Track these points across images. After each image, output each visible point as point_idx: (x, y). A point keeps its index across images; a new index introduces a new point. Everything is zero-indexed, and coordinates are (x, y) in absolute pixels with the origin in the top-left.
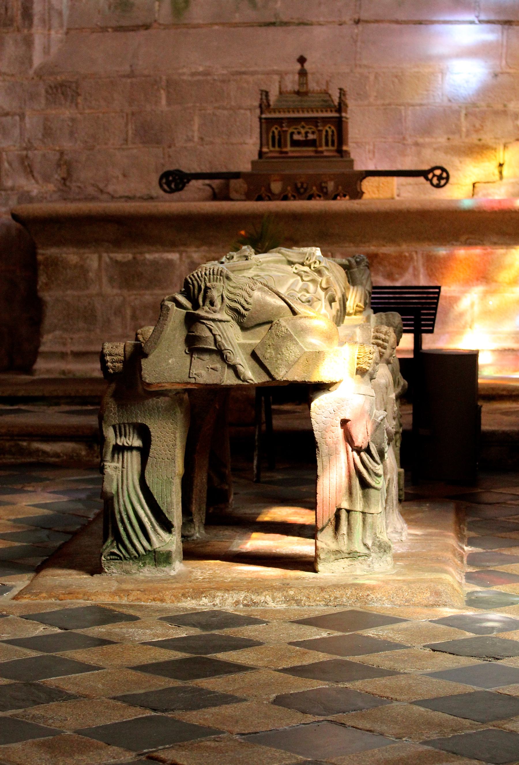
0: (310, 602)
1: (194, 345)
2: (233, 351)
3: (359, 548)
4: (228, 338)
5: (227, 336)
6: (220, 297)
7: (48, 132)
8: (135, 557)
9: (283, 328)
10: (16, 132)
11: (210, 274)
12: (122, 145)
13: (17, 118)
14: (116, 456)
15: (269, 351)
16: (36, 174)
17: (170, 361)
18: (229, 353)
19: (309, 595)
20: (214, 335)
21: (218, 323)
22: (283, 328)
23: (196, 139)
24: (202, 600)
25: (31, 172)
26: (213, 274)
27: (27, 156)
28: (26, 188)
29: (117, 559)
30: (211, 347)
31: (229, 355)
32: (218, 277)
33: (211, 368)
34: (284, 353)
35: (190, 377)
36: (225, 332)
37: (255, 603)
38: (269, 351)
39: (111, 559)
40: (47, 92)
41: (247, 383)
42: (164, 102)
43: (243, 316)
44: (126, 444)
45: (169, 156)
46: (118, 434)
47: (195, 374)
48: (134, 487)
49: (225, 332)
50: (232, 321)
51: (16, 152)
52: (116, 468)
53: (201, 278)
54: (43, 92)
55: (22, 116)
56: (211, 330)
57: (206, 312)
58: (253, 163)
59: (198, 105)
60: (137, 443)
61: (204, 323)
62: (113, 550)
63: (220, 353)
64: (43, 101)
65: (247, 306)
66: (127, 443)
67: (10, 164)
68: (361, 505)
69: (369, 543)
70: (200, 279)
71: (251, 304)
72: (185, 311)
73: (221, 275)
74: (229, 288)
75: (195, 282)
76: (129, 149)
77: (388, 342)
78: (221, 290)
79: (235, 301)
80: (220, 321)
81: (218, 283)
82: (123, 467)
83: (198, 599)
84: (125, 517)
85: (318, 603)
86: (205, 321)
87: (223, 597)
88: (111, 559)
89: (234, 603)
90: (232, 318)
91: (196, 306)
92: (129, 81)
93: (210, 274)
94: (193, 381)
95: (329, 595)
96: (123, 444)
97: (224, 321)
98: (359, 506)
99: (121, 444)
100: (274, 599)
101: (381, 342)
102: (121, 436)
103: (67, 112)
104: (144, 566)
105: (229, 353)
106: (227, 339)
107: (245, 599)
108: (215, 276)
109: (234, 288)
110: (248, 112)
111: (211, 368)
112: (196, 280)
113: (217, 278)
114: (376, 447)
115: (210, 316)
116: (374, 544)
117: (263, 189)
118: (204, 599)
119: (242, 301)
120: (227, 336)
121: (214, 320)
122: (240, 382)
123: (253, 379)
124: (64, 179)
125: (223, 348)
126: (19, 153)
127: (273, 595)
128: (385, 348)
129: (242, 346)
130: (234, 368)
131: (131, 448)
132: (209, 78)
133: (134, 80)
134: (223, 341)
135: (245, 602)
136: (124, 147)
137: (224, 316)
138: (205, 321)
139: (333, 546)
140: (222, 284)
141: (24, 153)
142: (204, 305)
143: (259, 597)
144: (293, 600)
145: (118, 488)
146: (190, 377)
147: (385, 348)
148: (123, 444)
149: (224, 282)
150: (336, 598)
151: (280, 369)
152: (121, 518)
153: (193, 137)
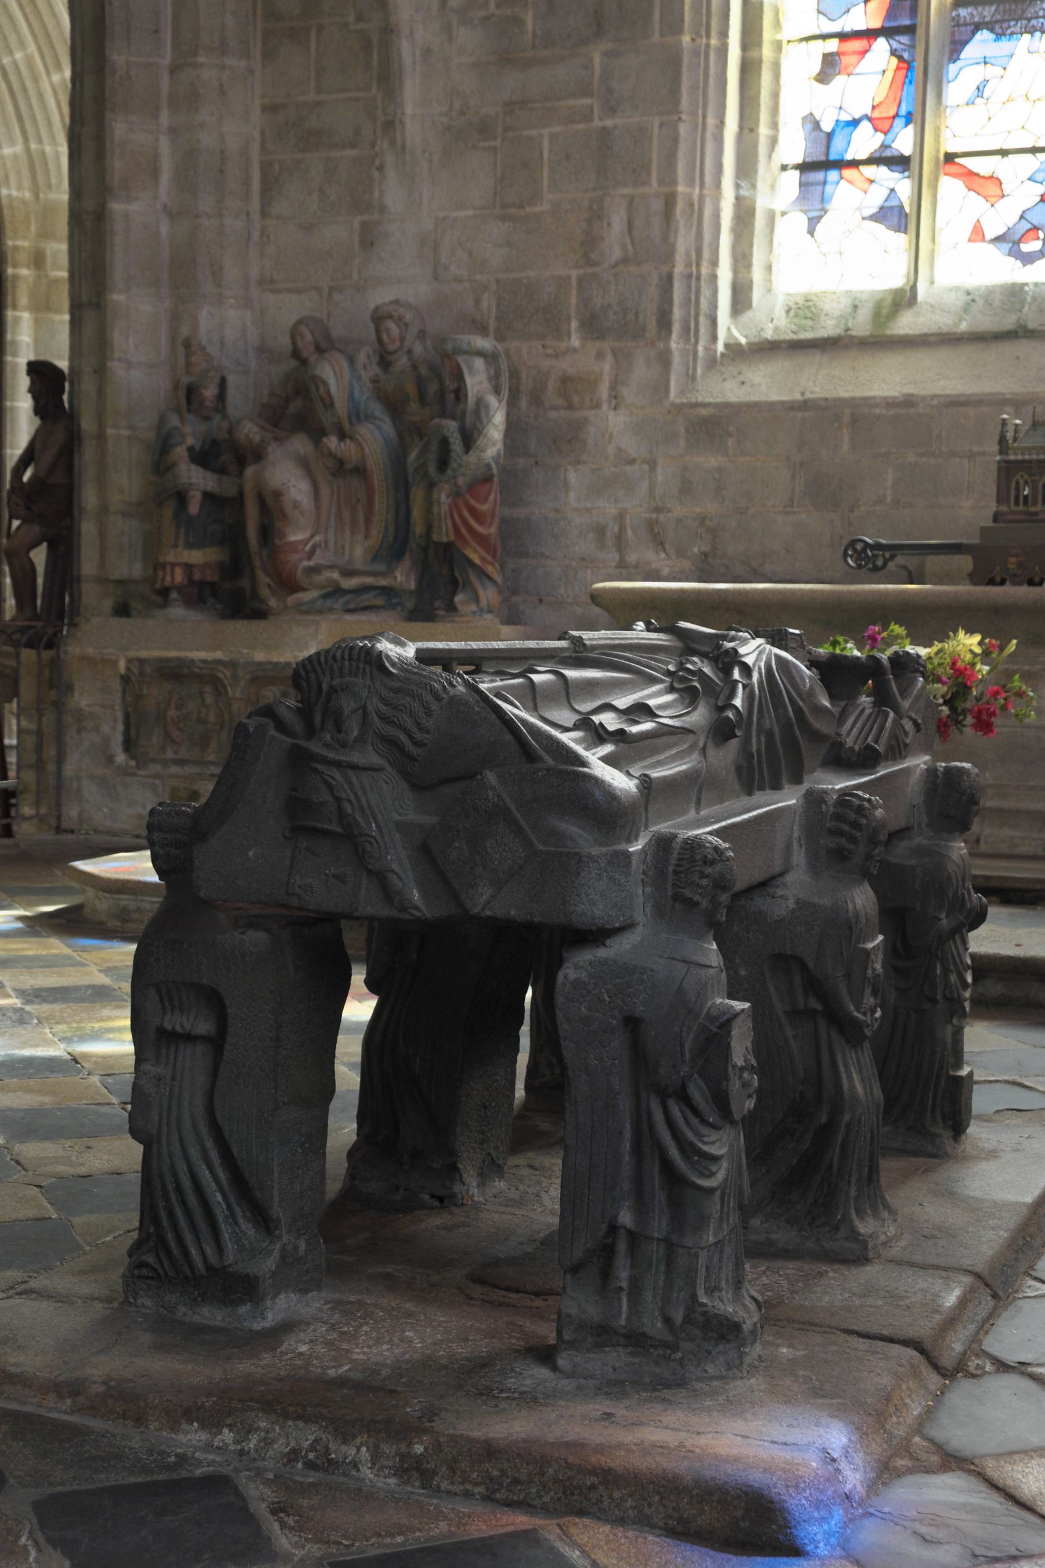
0: (452, 1483)
1: (302, 820)
2: (379, 839)
3: (653, 1326)
4: (370, 808)
5: (368, 803)
6: (361, 711)
7: (686, 489)
8: (186, 1277)
9: (490, 793)
10: (644, 486)
11: (343, 658)
12: (785, 507)
13: (646, 467)
14: (164, 1051)
15: (456, 844)
16: (667, 546)
17: (251, 854)
18: (370, 843)
19: (456, 1461)
20: (338, 800)
21: (350, 773)
22: (490, 793)
23: (889, 499)
24: (221, 1433)
25: (662, 544)
26: (351, 659)
27: (657, 521)
28: (653, 566)
29: (152, 1278)
30: (330, 828)
31: (368, 848)
32: (361, 665)
33: (334, 876)
34: (490, 850)
35: (288, 894)
36: (365, 793)
37: (330, 1462)
38: (456, 844)
39: (140, 1277)
40: (687, 431)
41: (407, 917)
42: (846, 447)
43: (413, 759)
44: (178, 1029)
45: (850, 524)
46: (167, 1003)
47: (300, 887)
48: (194, 1126)
49: (365, 793)
50: (390, 769)
51: (644, 515)
52: (159, 1079)
53: (324, 666)
54: (682, 430)
55: (652, 464)
56: (330, 788)
57: (327, 746)
58: (984, 530)
59: (894, 450)
60: (204, 1027)
61: (316, 770)
62: (144, 1258)
63: (350, 838)
64: (682, 443)
65: (418, 736)
66: (182, 1026)
67: (635, 533)
68: (664, 1223)
69: (678, 1317)
70: (322, 669)
71: (428, 732)
72: (289, 740)
73: (366, 662)
74: (383, 691)
75: (312, 676)
76: (795, 513)
77: (861, 831)
78: (365, 693)
79: (394, 722)
80: (354, 767)
81: (359, 681)
82: (173, 1079)
83: (214, 1430)
84: (170, 1187)
85: (469, 1487)
86: (320, 767)
87: (267, 1432)
88: (140, 1277)
89: (288, 1453)
90: (389, 761)
91: (311, 732)
92: (799, 415)
93: (343, 658)
94: (295, 902)
95: (502, 1470)
96: (173, 1028)
97: (365, 769)
98: (659, 1226)
99: (169, 1027)
100: (376, 1456)
101: (846, 828)
102: (173, 1008)
103: (713, 461)
104: (203, 1300)
105: (370, 843)
106: (368, 811)
107: (312, 1448)
108: (354, 664)
109: (396, 691)
110: (966, 461)
111: (334, 876)
112: (315, 670)
113: (358, 668)
114: (709, 1088)
115: (331, 755)
116: (688, 1319)
117: (998, 568)
118: (226, 1431)
119: (409, 723)
120: (368, 803)
121: (338, 764)
122: (395, 913)
123: (423, 908)
124: (706, 555)
125: (356, 832)
126: (648, 515)
127: (376, 1447)
128: (853, 840)
129: (403, 828)
130: (380, 878)
131: (190, 1038)
132: (912, 410)
133: (807, 414)
134: (358, 816)
135: (311, 1456)
136: (789, 509)
137: (371, 757)
138: (320, 767)
139: (593, 1312)
140: (368, 682)
141: (655, 516)
142: (322, 729)
143: (344, 1448)
144: (417, 1469)
145: (160, 1123)
146: (288, 894)
147: (853, 840)
148: (173, 1028)
149: (372, 679)
150: (516, 1481)
151: (480, 890)
152: (164, 1188)
153: (885, 496)
